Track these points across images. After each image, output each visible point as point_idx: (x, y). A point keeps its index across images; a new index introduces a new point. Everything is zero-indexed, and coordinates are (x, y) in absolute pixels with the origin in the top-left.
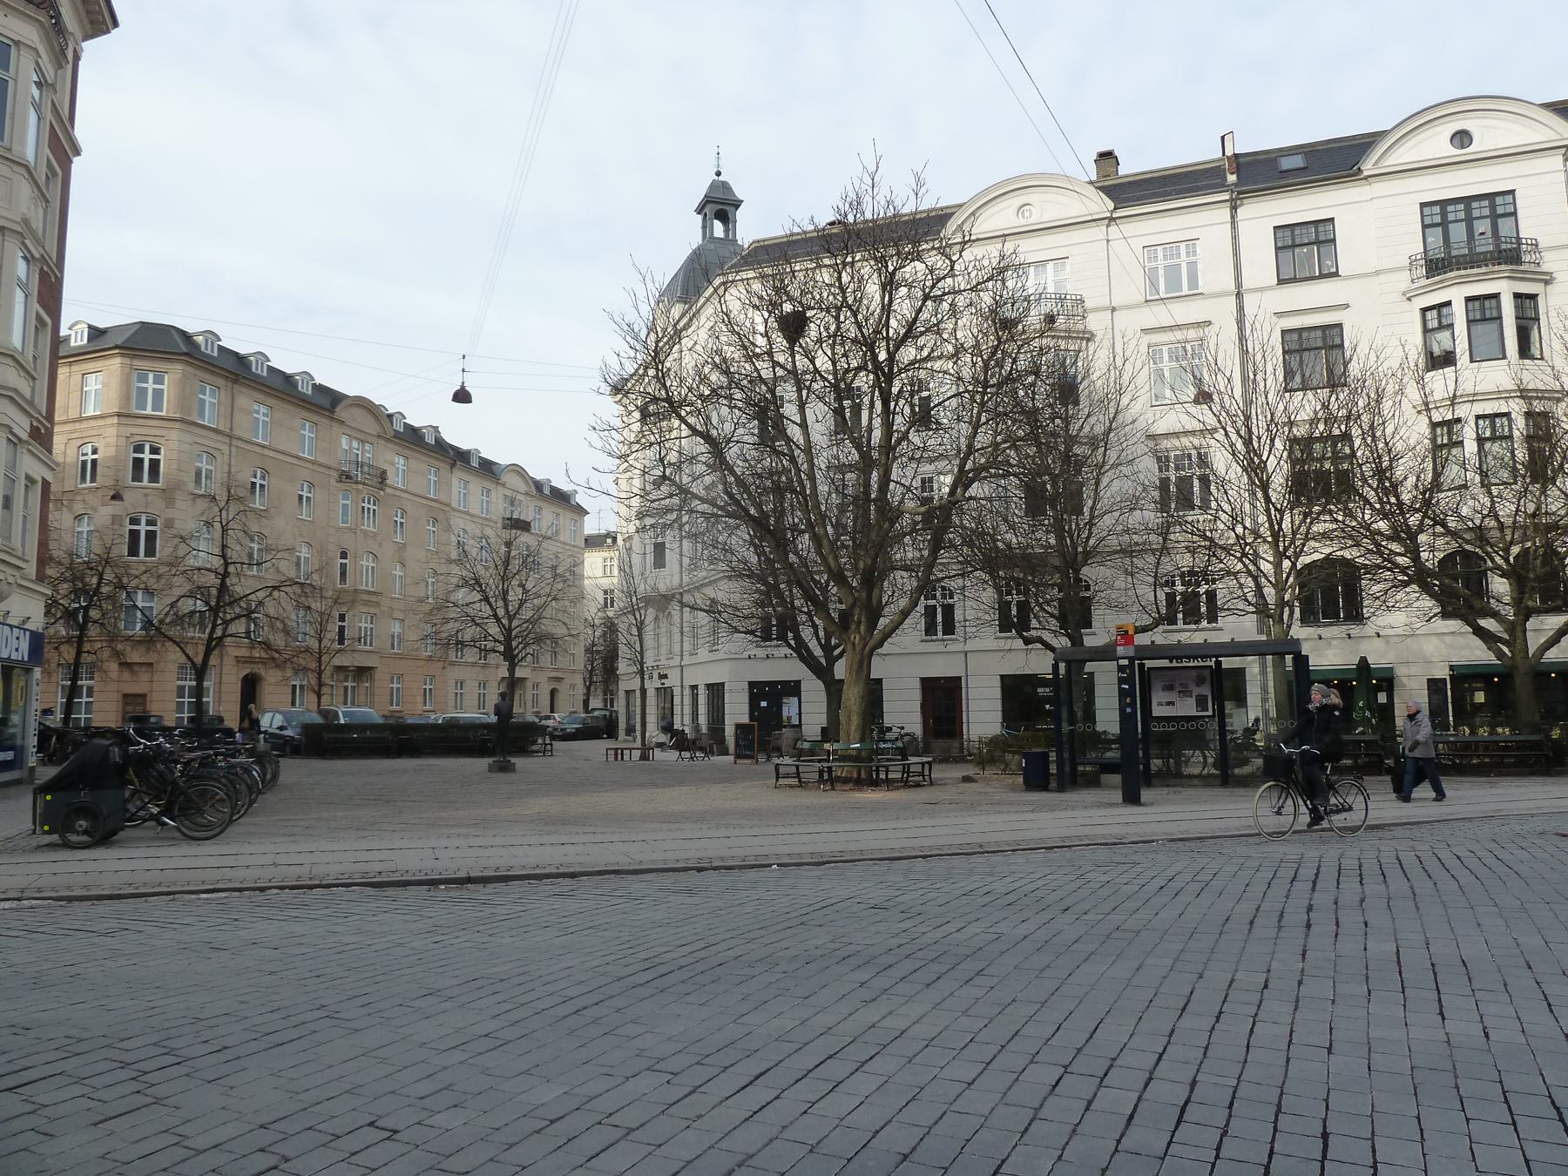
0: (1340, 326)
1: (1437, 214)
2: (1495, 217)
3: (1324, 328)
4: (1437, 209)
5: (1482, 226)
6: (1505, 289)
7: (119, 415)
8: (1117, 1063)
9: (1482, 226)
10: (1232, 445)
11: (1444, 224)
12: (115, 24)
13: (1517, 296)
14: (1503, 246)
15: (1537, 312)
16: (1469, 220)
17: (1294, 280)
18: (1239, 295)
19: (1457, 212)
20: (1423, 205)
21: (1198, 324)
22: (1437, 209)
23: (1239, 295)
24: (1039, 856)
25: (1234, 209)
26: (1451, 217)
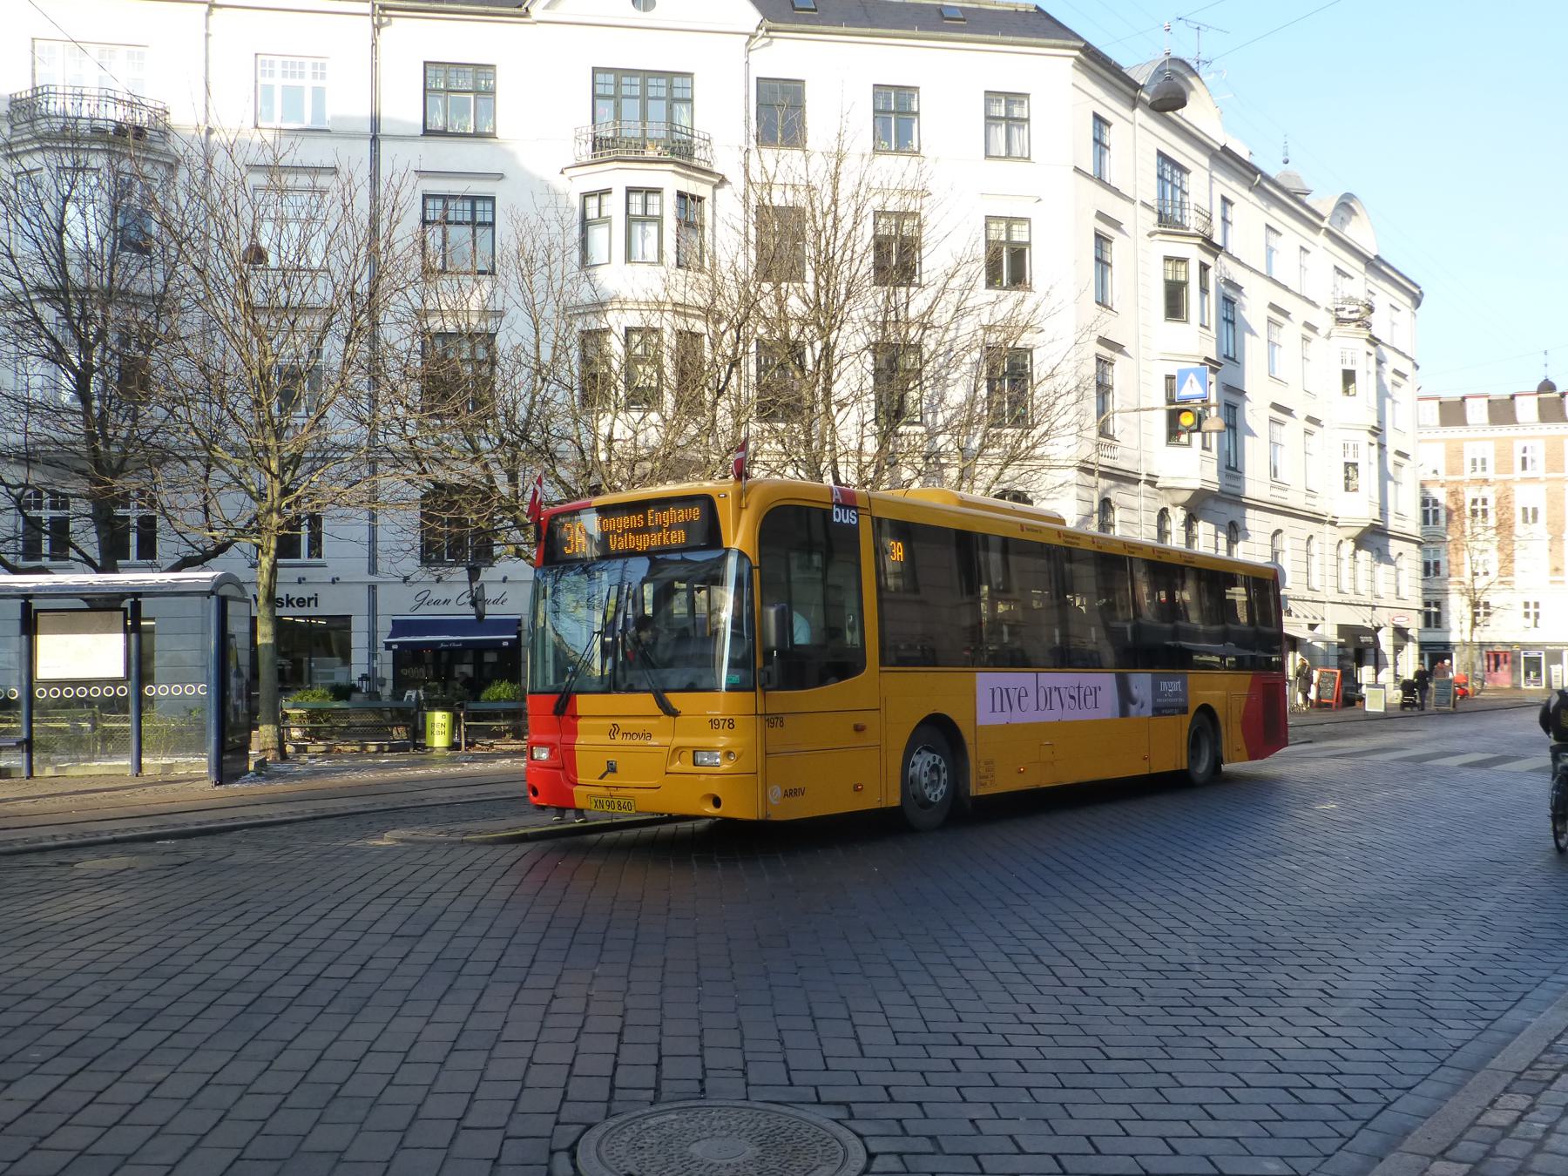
0: (492, 199)
1: (611, 85)
2: (672, 101)
3: (474, 199)
4: (611, 78)
5: (657, 110)
6: (670, 181)
7: (375, 122)
8: (477, 1096)
9: (657, 110)
10: (746, 234)
11: (617, 98)
12: (803, 82)
13: (681, 196)
14: (677, 136)
15: (702, 219)
16: (644, 99)
17: (443, 133)
18: (375, 140)
19: (632, 87)
20: (595, 70)
21: (317, 170)
22: (611, 78)
23: (375, 140)
24: (76, 1109)
25: (377, 27)
26: (625, 91)
